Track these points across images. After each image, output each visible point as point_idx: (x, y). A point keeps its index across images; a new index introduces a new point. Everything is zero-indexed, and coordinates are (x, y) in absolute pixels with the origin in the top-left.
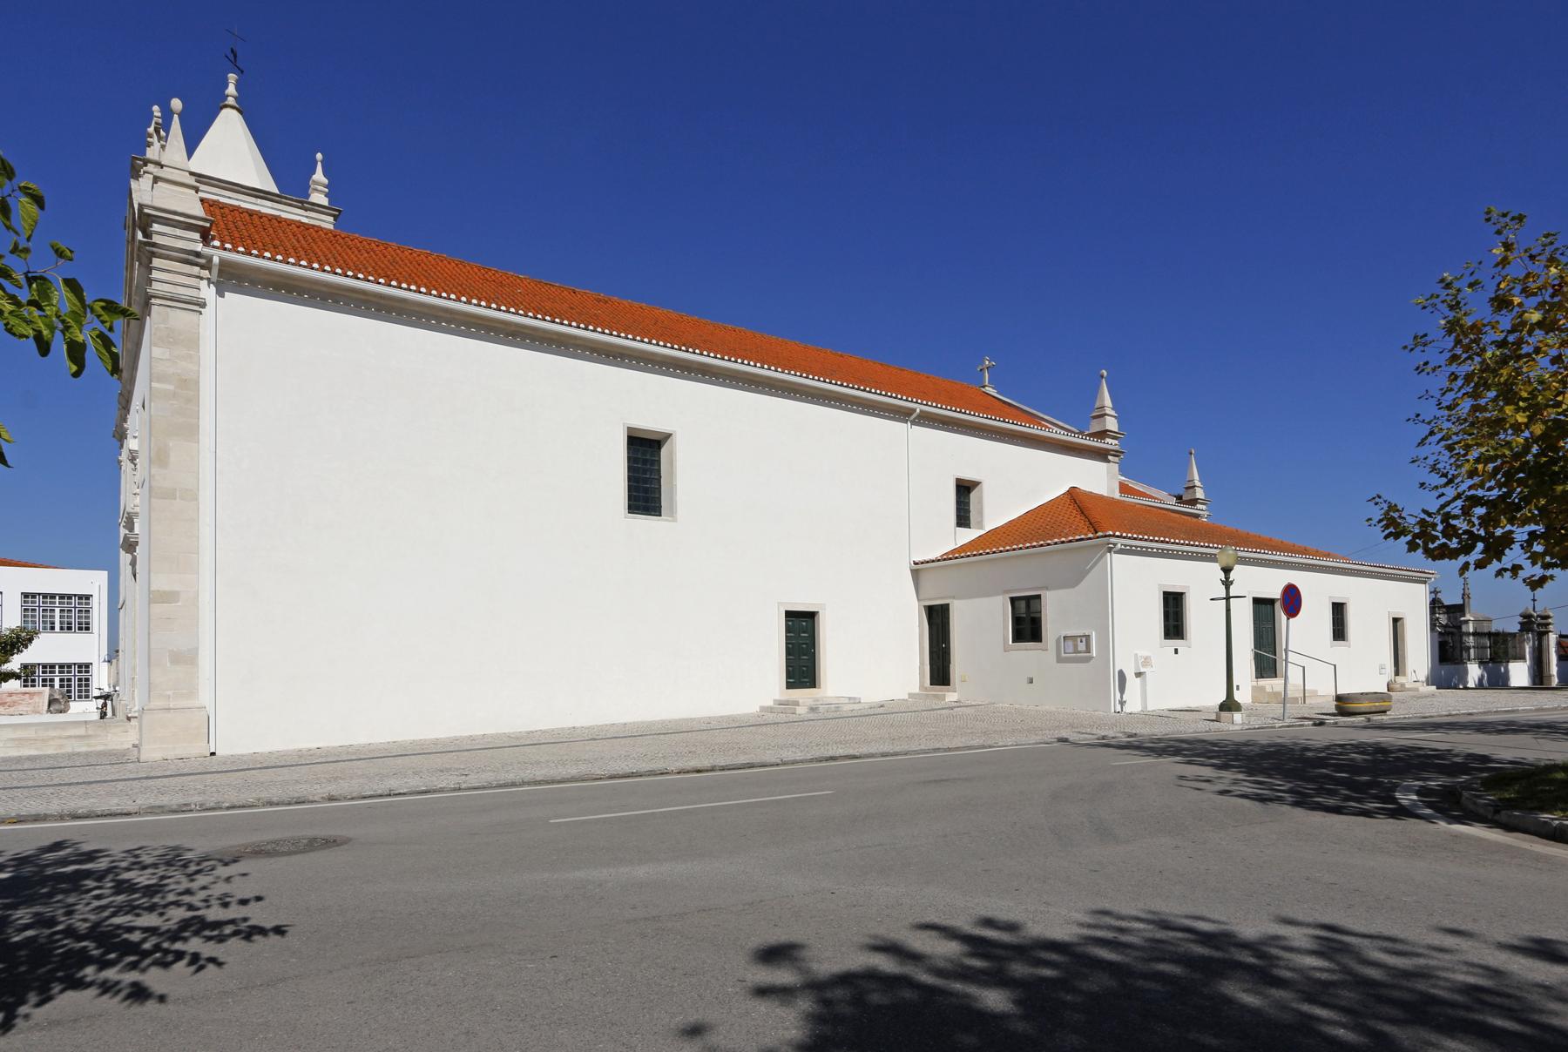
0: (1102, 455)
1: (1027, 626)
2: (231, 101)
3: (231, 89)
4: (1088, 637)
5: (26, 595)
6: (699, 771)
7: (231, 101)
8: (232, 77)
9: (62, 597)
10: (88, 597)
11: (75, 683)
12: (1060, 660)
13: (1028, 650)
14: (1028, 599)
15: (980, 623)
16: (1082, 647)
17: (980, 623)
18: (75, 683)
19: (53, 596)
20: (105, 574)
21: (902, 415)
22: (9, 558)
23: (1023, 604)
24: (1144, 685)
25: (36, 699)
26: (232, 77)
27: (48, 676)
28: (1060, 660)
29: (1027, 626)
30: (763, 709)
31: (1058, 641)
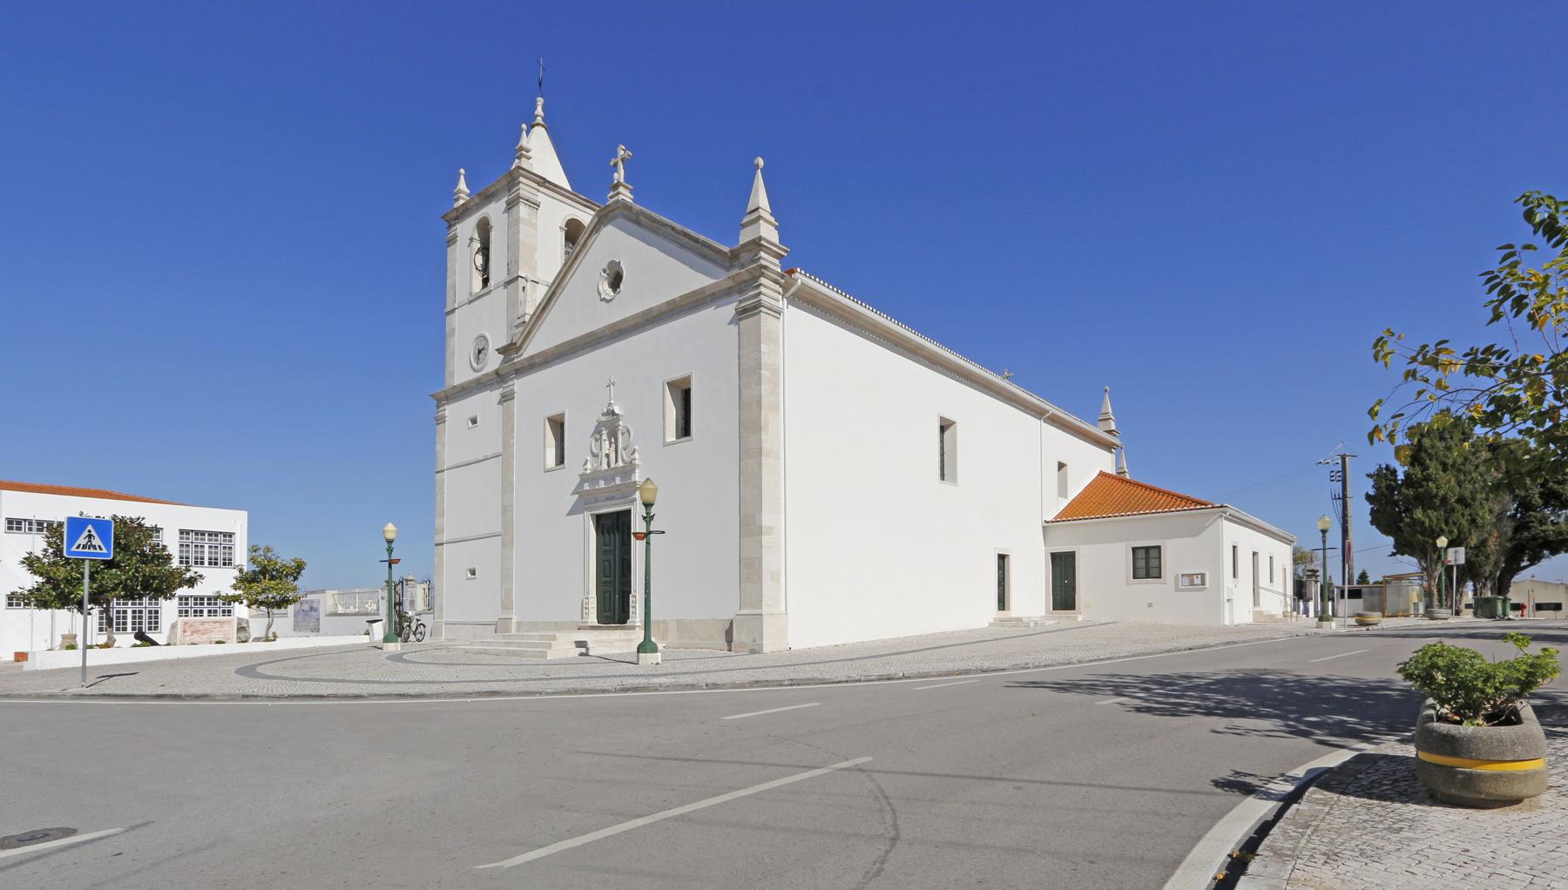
0: (1108, 447)
1: (1147, 563)
2: (539, 120)
3: (539, 111)
4: (1203, 575)
5: (182, 532)
6: (983, 671)
7: (539, 120)
8: (540, 101)
9: (210, 534)
10: (230, 535)
11: (145, 615)
12: (1177, 590)
13: (1147, 586)
14: (1147, 549)
15: (1103, 562)
16: (1197, 581)
17: (1103, 562)
18: (145, 615)
19: (203, 533)
20: (245, 513)
21: (1039, 413)
22: (109, 490)
23: (1142, 554)
24: (1231, 607)
25: (226, 627)
26: (540, 101)
27: (198, 608)
28: (1177, 590)
29: (1147, 563)
30: (991, 625)
31: (1176, 577)
